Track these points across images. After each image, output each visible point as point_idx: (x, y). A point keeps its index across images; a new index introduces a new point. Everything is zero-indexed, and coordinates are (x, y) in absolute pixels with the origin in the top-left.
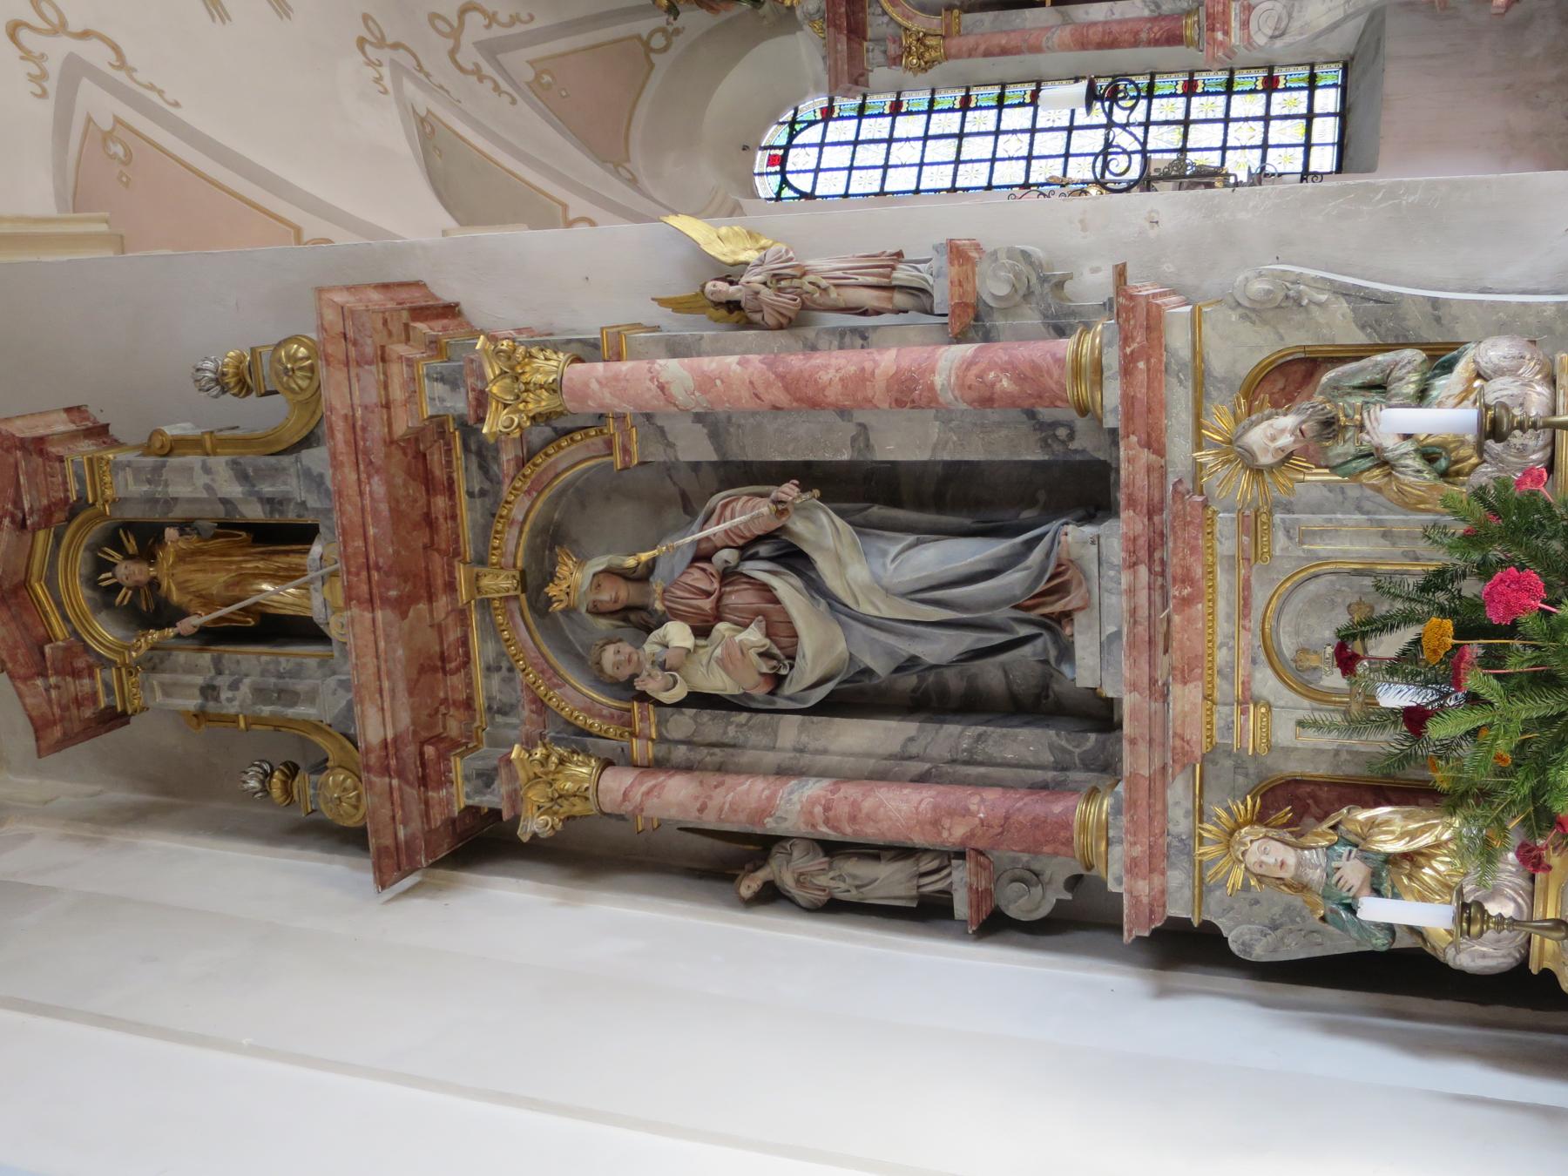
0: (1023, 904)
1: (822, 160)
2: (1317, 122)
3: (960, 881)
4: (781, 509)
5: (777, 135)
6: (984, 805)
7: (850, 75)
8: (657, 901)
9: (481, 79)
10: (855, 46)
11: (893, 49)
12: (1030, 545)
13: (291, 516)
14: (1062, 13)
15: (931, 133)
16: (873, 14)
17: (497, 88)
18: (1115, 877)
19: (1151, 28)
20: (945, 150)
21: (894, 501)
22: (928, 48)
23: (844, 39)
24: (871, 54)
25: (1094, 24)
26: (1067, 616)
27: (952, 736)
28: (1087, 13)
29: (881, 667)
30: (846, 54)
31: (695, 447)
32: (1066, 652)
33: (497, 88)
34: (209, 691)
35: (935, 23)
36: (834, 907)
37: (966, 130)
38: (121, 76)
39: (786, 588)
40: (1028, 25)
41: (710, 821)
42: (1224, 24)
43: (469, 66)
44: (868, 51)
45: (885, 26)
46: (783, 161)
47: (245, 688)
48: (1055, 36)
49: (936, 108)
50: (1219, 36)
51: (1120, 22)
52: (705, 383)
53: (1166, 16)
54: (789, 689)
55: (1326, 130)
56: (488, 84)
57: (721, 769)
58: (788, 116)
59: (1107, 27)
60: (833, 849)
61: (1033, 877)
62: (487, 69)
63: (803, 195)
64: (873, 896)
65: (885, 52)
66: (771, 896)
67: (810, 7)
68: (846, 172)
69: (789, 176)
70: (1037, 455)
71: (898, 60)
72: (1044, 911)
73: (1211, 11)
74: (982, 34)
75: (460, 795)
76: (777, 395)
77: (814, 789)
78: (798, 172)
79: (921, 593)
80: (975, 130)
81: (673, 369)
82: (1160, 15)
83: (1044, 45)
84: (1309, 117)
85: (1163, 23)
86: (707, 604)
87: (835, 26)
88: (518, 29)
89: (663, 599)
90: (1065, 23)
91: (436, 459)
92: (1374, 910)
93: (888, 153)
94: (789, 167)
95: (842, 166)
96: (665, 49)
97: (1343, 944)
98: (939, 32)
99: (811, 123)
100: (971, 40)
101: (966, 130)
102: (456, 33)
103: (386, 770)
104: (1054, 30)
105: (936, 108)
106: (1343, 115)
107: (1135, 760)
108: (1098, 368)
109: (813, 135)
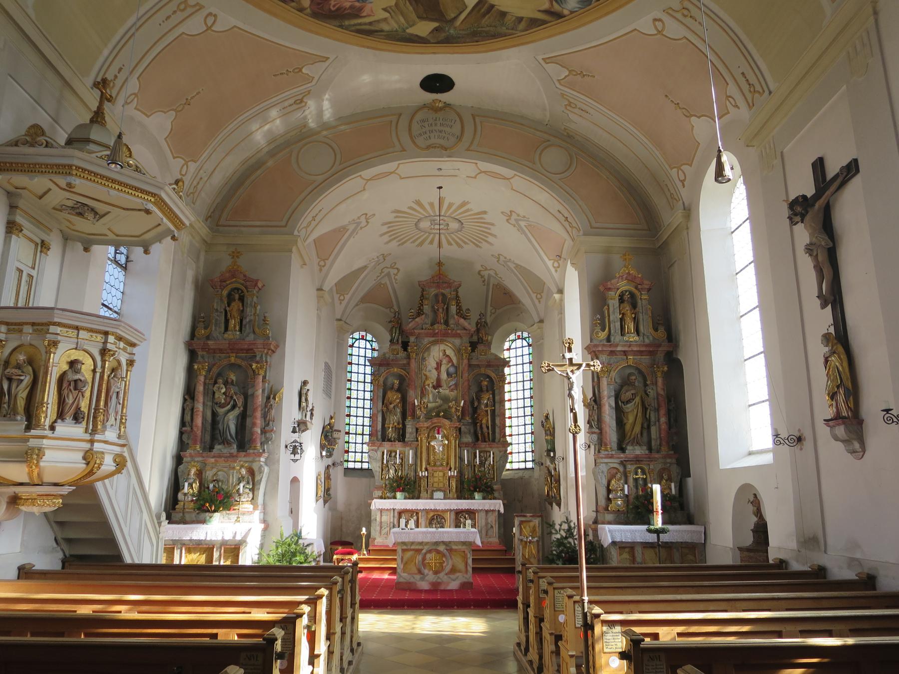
0: (185, 437)
2: (360, 464)
3: (187, 428)
4: (239, 408)
5: (369, 337)
6: (199, 433)
8: (185, 388)
9: (381, 273)
12: (234, 439)
13: (243, 329)
17: (378, 276)
20: (361, 378)
21: (242, 419)
26: (224, 444)
27: (209, 428)
29: (218, 418)
31: (250, 392)
32: (220, 444)
33: (378, 276)
34: (217, 310)
35: (381, 382)
36: (183, 410)
38: (359, 228)
39: (229, 407)
41: (196, 393)
43: (383, 271)
47: (217, 317)
51: (377, 423)
52: (257, 396)
54: (215, 405)
55: (358, 466)
56: (379, 275)
58: (374, 340)
60: (192, 410)
61: (188, 438)
62: (383, 274)
64: (185, 415)
66: (185, 400)
70: (246, 440)
72: (184, 440)
75: (200, 353)
76: (255, 407)
77: (201, 409)
79: (228, 426)
81: (260, 391)
84: (362, 462)
86: (228, 394)
88: (394, 281)
90: (378, 411)
92: (186, 484)
94: (361, 341)
96: (391, 311)
97: (181, 480)
99: (371, 346)
102: (392, 267)
106: (362, 469)
107: (205, 454)
108: (255, 449)
109: (369, 346)
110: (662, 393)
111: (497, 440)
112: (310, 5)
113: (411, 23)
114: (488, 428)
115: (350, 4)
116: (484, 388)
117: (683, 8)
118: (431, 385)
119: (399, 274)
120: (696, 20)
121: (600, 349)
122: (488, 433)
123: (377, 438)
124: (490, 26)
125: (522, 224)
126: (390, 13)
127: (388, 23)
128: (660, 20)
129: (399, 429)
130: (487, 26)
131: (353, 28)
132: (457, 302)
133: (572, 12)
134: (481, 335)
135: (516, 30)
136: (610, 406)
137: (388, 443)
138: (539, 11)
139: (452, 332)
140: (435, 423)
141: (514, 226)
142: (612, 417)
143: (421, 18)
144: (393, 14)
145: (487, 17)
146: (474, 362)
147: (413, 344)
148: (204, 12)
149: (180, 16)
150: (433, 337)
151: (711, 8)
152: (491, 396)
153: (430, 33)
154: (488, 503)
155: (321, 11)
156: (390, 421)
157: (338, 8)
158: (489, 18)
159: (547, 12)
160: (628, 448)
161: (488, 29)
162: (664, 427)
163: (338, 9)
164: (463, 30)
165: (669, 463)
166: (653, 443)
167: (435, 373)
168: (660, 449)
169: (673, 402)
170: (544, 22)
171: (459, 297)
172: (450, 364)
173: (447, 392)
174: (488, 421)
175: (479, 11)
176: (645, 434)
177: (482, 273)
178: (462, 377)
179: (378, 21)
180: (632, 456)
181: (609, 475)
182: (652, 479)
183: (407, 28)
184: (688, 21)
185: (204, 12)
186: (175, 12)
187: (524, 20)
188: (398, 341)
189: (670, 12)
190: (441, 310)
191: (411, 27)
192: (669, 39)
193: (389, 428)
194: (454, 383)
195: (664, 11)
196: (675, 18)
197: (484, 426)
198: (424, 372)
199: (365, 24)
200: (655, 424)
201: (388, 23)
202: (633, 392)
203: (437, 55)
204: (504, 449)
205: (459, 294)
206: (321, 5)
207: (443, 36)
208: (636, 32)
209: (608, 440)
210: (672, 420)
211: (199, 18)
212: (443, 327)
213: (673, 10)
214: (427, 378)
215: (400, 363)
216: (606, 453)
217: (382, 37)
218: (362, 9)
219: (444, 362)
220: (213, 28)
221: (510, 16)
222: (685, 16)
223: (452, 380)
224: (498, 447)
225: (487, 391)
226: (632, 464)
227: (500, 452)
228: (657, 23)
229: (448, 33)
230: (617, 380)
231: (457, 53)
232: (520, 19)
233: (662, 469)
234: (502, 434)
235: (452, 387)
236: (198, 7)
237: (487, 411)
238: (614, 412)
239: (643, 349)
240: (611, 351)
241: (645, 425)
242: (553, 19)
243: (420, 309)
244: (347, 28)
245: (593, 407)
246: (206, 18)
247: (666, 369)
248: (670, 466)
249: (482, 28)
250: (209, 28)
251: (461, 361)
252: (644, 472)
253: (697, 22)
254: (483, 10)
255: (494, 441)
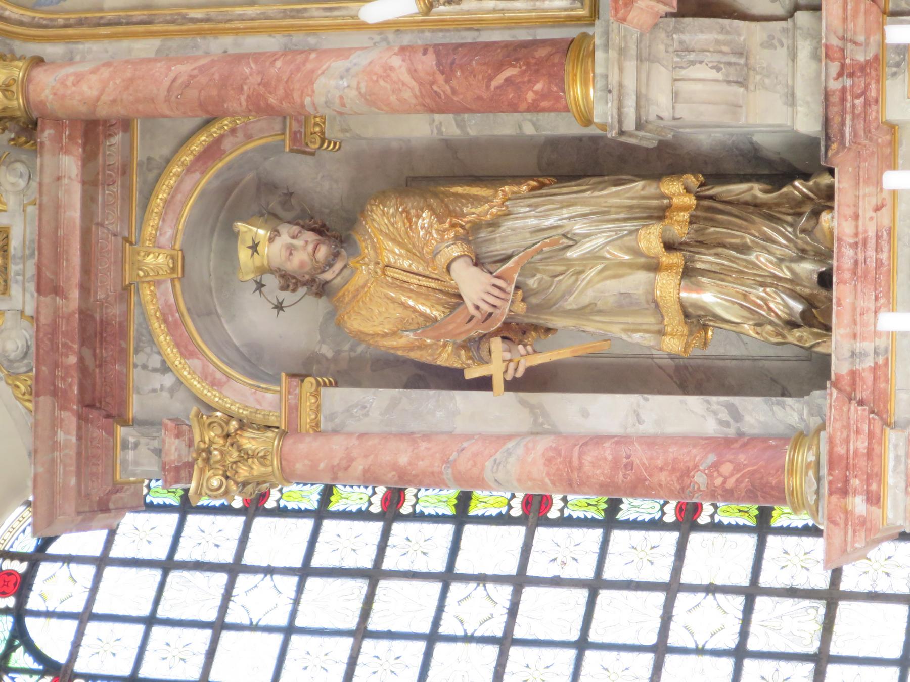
1: (98, 596)
7: (83, 495)
10: (97, 433)
11: (174, 449)
14: (532, 408)
15: (316, 563)
16: (144, 367)
19: (716, 466)
22: (246, 456)
23: (70, 420)
24: (131, 455)
25: (598, 439)
28: (585, 414)
30: (73, 452)
37: (387, 565)
40: (461, 426)
42: (869, 478)
44: (125, 446)
45: (165, 394)
48: (512, 460)
49: (333, 507)
50: (858, 504)
51: (651, 441)
53: (754, 439)
59: (623, 451)
63: (49, 666)
65: (158, 452)
67: (10, 346)
68: (140, 628)
69: (30, 623)
71: (184, 474)
73: (840, 450)
74: (362, 436)
78: (49, 614)
80: (404, 566)
82: (741, 435)
83: (488, 475)
85: (742, 458)
87: (55, 393)
89: (661, 291)
93: (227, 596)
94: (34, 602)
95: (134, 613)
98: (273, 421)
100: (337, 446)
101: (387, 565)
104: (510, 445)
105: (333, 507)
123: (799, 438)
215: (74, 213)
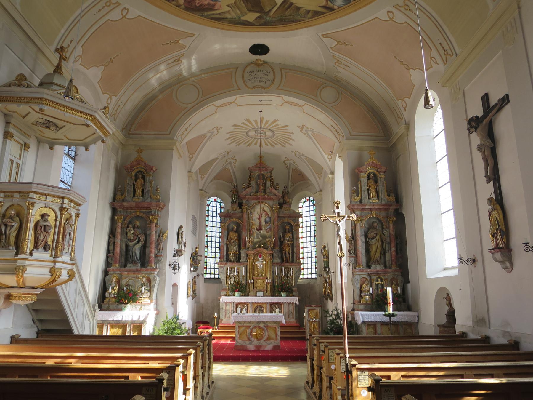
0: (109, 259)
2: (214, 275)
3: (111, 254)
4: (142, 242)
5: (219, 200)
6: (118, 257)
8: (110, 230)
9: (226, 162)
12: (139, 261)
13: (144, 195)
17: (224, 164)
18: (112, 268)
20: (214, 224)
21: (143, 249)
26: (133, 264)
27: (124, 254)
29: (129, 248)
31: (148, 233)
32: (130, 263)
33: (224, 164)
34: (129, 184)
35: (226, 227)
36: (109, 243)
38: (213, 135)
39: (136, 241)
41: (116, 233)
43: (227, 161)
46: (215, 201)
47: (129, 188)
52: (153, 235)
54: (128, 241)
55: (212, 276)
56: (225, 163)
57: (121, 233)
58: (222, 202)
60: (114, 243)
61: (112, 260)
62: (227, 163)
64: (110, 246)
66: (110, 237)
70: (146, 261)
72: (109, 261)
75: (119, 210)
79: (135, 253)
81: (154, 232)
84: (214, 274)
86: (135, 234)
88: (234, 167)
90: (224, 244)
91: (149, 209)
92: (110, 287)
94: (214, 202)
96: (232, 185)
97: (107, 285)
99: (220, 205)
102: (232, 159)
103: (121, 204)
106: (214, 278)
107: (121, 269)
110: (392, 233)
111: (294, 261)
112: (184, 3)
113: (244, 14)
114: (289, 254)
115: (208, 2)
116: (287, 230)
117: (405, 5)
118: (255, 229)
119: (236, 163)
120: (413, 12)
121: (356, 207)
122: (290, 257)
123: (224, 260)
124: (291, 16)
125: (310, 133)
126: (231, 8)
127: (230, 14)
128: (391, 12)
129: (237, 255)
130: (289, 15)
131: (209, 17)
132: (271, 179)
133: (339, 7)
134: (285, 199)
135: (306, 18)
136: (362, 241)
137: (230, 263)
138: (320, 6)
139: (268, 197)
140: (258, 251)
141: (305, 134)
142: (363, 248)
143: (249, 11)
144: (233, 8)
145: (289, 10)
146: (281, 215)
147: (245, 204)
148: (121, 7)
149: (107, 9)
150: (257, 200)
151: (422, 5)
152: (291, 235)
153: (255, 20)
154: (290, 299)
155: (190, 7)
156: (231, 250)
157: (200, 5)
158: (290, 11)
159: (324, 7)
160: (373, 266)
161: (289, 17)
162: (394, 253)
163: (200, 6)
164: (275, 18)
165: (397, 275)
166: (387, 263)
167: (258, 221)
168: (391, 266)
169: (399, 239)
170: (323, 13)
171: (272, 176)
172: (267, 216)
173: (265, 233)
174: (289, 250)
175: (284, 6)
176: (382, 258)
177: (286, 162)
178: (274, 224)
179: (224, 13)
180: (375, 271)
181: (361, 282)
182: (387, 284)
183: (242, 17)
184: (408, 12)
185: (121, 7)
186: (104, 7)
187: (311, 12)
188: (236, 202)
189: (397, 7)
190: (261, 184)
191: (244, 16)
192: (396, 23)
193: (231, 254)
194: (269, 227)
195: (394, 7)
196: (400, 10)
197: (287, 253)
198: (251, 221)
199: (216, 14)
200: (388, 252)
201: (230, 14)
202: (375, 232)
203: (259, 33)
204: (299, 266)
205: (272, 175)
206: (190, 3)
207: (262, 21)
208: (377, 19)
209: (361, 261)
210: (398, 249)
211: (118, 11)
212: (263, 194)
213: (399, 6)
214: (253, 224)
215: (237, 215)
216: (360, 269)
217: (227, 22)
218: (215, 5)
219: (263, 215)
220: (126, 17)
221: (303, 10)
222: (406, 10)
223: (268, 226)
224: (295, 266)
225: (289, 232)
226: (374, 275)
227: (297, 268)
228: (389, 14)
229: (266, 20)
230: (366, 226)
231: (271, 31)
232: (308, 12)
233: (393, 278)
234: (298, 258)
235: (268, 230)
236: (117, 4)
237: (289, 244)
238: (364, 245)
239: (381, 207)
240: (362, 208)
241: (383, 252)
242: (328, 11)
243: (249, 183)
244: (206, 17)
245: (352, 242)
246: (122, 10)
247: (395, 219)
248: (397, 277)
249: (286, 16)
250: (124, 17)
251: (273, 214)
252: (382, 280)
253: (413, 13)
254: (286, 6)
255: (293, 261)
